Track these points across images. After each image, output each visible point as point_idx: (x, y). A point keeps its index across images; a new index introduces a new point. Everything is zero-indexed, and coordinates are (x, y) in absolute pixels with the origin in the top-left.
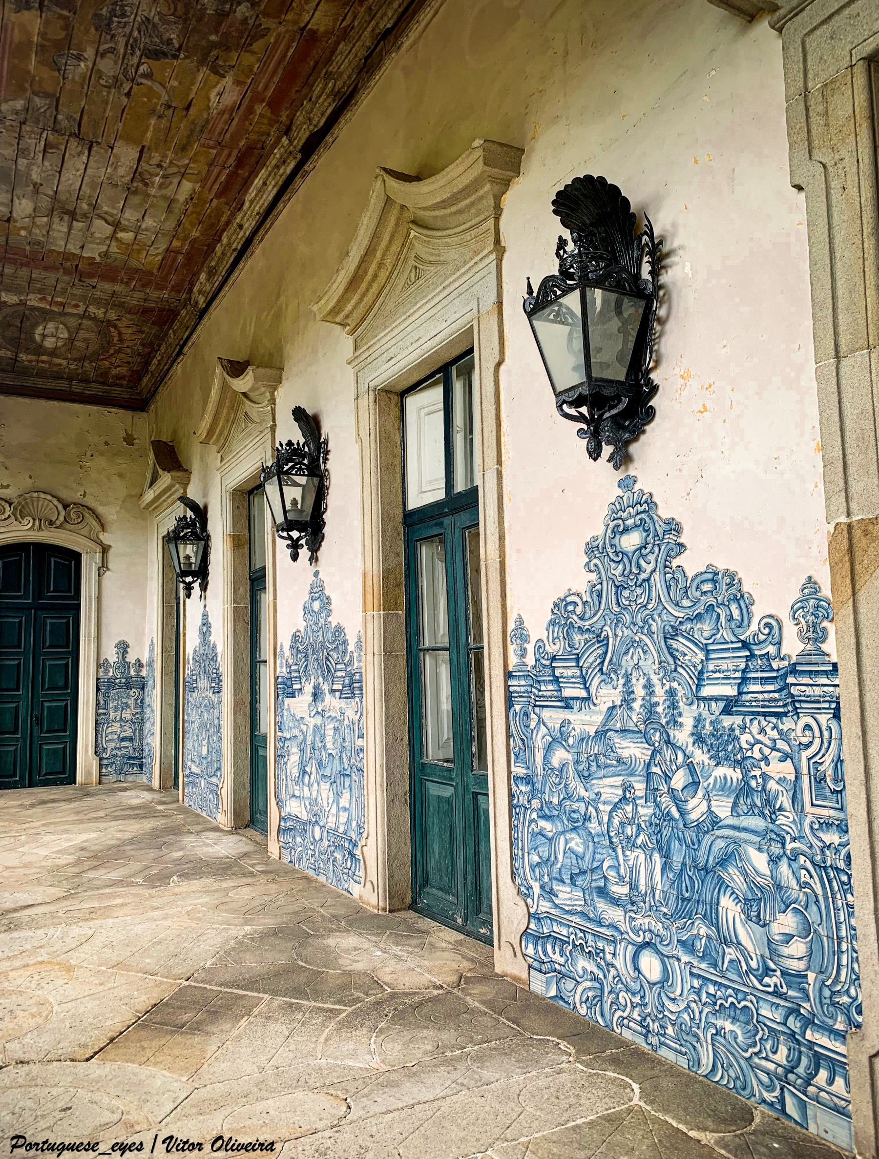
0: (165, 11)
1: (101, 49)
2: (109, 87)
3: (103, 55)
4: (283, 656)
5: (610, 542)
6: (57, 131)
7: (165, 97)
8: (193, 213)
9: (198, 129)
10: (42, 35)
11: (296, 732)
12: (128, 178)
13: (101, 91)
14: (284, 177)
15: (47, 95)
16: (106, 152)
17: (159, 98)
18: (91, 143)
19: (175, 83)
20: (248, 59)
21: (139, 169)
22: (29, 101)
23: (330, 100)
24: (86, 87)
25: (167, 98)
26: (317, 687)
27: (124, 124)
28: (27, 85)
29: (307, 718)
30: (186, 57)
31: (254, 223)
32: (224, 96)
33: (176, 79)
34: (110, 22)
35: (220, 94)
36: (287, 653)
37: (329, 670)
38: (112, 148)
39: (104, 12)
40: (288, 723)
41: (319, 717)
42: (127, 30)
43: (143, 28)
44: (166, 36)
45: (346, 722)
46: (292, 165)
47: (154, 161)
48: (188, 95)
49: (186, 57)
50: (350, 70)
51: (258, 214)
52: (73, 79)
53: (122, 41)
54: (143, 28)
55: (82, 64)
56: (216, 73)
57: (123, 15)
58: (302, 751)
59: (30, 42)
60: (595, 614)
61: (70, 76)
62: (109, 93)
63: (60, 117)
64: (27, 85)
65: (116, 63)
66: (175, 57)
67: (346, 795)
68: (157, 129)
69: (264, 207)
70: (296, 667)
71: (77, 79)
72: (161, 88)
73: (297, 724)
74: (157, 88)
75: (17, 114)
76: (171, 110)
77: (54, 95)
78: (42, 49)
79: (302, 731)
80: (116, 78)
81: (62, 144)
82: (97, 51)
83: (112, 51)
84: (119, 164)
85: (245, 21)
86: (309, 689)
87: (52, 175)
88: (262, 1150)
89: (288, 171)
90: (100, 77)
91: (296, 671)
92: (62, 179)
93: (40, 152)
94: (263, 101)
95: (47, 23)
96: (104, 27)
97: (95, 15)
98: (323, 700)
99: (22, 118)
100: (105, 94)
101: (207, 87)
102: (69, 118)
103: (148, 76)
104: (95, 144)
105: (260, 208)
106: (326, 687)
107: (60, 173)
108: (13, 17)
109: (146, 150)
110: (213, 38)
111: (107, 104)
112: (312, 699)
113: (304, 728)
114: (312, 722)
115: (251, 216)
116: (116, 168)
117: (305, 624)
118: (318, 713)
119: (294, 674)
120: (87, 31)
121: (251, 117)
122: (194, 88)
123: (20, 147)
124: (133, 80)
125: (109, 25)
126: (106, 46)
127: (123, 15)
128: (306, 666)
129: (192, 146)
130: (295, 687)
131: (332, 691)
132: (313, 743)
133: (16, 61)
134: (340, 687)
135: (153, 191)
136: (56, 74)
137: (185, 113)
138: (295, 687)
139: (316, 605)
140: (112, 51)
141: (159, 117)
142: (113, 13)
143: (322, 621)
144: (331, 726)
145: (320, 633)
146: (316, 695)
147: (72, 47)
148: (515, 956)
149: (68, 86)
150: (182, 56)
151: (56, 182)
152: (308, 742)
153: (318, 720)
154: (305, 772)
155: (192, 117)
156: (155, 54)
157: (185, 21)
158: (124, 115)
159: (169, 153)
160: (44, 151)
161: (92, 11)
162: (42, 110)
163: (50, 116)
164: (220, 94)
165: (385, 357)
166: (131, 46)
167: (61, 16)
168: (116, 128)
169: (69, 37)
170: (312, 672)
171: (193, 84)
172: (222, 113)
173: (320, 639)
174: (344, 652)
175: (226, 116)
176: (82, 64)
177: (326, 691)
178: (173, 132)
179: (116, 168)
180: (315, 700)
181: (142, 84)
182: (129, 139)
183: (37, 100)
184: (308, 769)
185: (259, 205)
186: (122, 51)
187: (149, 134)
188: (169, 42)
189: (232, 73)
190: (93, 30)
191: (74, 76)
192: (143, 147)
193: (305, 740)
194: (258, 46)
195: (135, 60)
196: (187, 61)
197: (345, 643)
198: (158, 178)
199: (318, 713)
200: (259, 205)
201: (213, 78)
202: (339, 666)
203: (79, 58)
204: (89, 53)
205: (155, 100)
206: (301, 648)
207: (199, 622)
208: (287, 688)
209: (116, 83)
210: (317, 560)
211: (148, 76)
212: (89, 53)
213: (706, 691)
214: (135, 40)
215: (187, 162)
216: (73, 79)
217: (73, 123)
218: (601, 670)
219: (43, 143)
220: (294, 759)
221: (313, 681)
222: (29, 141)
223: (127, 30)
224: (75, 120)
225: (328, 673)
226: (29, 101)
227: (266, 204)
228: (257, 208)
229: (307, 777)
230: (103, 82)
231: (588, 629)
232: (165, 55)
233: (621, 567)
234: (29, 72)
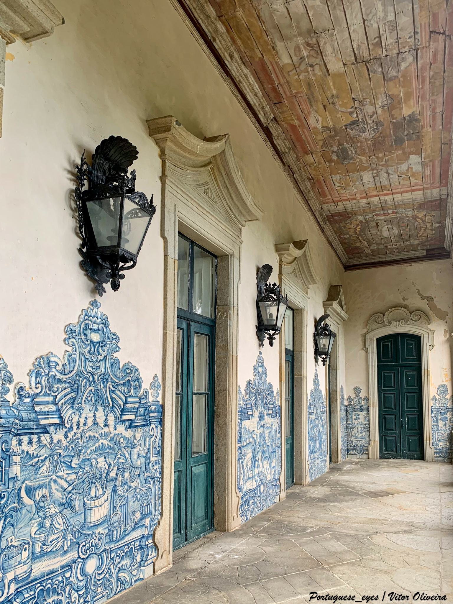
0: (360, 138)
1: (375, 114)
2: (364, 99)
3: (374, 113)
4: (241, 394)
5: (83, 332)
6: (378, 59)
7: (338, 107)
8: (262, 36)
9: (312, 99)
10: (401, 109)
11: (250, 440)
12: (322, 44)
13: (366, 95)
14: (258, 112)
15: (391, 79)
16: (346, 60)
17: (340, 105)
18: (357, 62)
19: (338, 116)
20: (320, 137)
21: (320, 56)
22: (398, 71)
23: (283, 150)
24: (374, 94)
25: (337, 107)
26: (261, 413)
27: (346, 83)
28: (401, 79)
29: (256, 430)
30: (342, 127)
31: (234, 74)
32: (315, 121)
33: (339, 118)
34: (377, 126)
35: (317, 120)
36: (243, 392)
37: (267, 404)
38: (344, 64)
39: (381, 128)
40: (245, 435)
41: (262, 428)
42: (369, 126)
43: (364, 129)
44: (354, 131)
45: (274, 428)
46: (262, 120)
47: (317, 68)
48: (329, 113)
49: (342, 127)
50: (289, 161)
51: (241, 82)
52: (381, 94)
53: (369, 121)
54: (364, 129)
55: (380, 104)
56: (326, 127)
57: (373, 130)
58: (254, 450)
59: (405, 103)
60: (69, 373)
61: (383, 95)
62: (363, 96)
63: (380, 70)
64: (401, 79)
65: (367, 112)
66: (346, 125)
67: (274, 460)
68: (329, 88)
69: (243, 88)
70: (250, 402)
71: (380, 96)
72: (343, 110)
73: (250, 435)
74: (344, 110)
75: (403, 58)
76: (330, 102)
77: (387, 81)
78: (400, 103)
79: (254, 438)
80: (364, 106)
81: (372, 50)
82: (377, 113)
83: (371, 117)
84: (334, 55)
85: (332, 146)
86: (257, 414)
87: (368, 15)
88: (323, 599)
89: (260, 116)
90: (370, 102)
91: (249, 403)
92: (360, 15)
93: (383, 34)
94: (299, 126)
95: (401, 114)
96: (378, 123)
97: (383, 125)
98: (264, 419)
99: (400, 57)
100: (364, 95)
101: (325, 119)
102: (375, 72)
103: (351, 113)
104: (354, 62)
105: (244, 86)
106: (265, 413)
107: (364, 21)
108: (414, 109)
109: (327, 74)
110: (338, 138)
111: (360, 89)
112: (258, 419)
113: (254, 436)
114: (258, 432)
115: (240, 75)
116: (334, 49)
117: (254, 377)
118: (261, 426)
119: (249, 406)
120: (384, 119)
121: (296, 118)
122: (329, 118)
123: (396, 32)
124: (356, 108)
125: (377, 125)
126: (374, 117)
127: (373, 130)
128: (256, 401)
129: (307, 89)
130: (249, 413)
131: (268, 414)
132: (259, 443)
133: (410, 90)
134: (271, 412)
135: (300, 40)
136: (390, 93)
137: (324, 104)
138: (249, 413)
139: (260, 370)
140: (371, 117)
141: (333, 95)
142: (377, 129)
143: (263, 379)
144: (268, 431)
145: (262, 385)
146: (261, 417)
147: (387, 110)
148: (169, 553)
149: (382, 89)
150: (344, 127)
151: (363, 9)
152: (257, 443)
153: (261, 430)
154: (255, 461)
155: (319, 103)
156: (354, 123)
157: (351, 138)
158: (349, 88)
159: (314, 78)
160: (380, 37)
161: (385, 126)
162: (390, 69)
163: (385, 67)
164: (317, 120)
165: (290, 290)
166: (364, 122)
167: (396, 118)
168: (349, 78)
169: (390, 112)
170: (259, 405)
171: (331, 119)
172: (309, 113)
173: (262, 388)
174: (273, 396)
175: (306, 112)
176: (380, 104)
177: (265, 415)
178: (321, 91)
179: (334, 49)
180: (260, 420)
181: (351, 108)
182: (340, 75)
183: (395, 74)
184: (257, 459)
185: (246, 86)
186: (367, 118)
187: (331, 84)
188: (352, 129)
189: (321, 130)
190: (382, 120)
191: (382, 97)
192: (329, 75)
193: (255, 443)
194: (321, 143)
195: (360, 117)
196: (340, 126)
197: (273, 392)
198: (305, 55)
199: (261, 426)
200: (246, 86)
201: (325, 125)
202: (271, 403)
203: (383, 106)
204: (379, 111)
205: (341, 103)
206: (252, 390)
207: (313, 377)
208: (244, 415)
209: (361, 103)
210: (263, 345)
211: (351, 113)
212: (379, 111)
213: (125, 418)
214: (364, 124)
215: (301, 77)
216: (381, 94)
217: (372, 69)
218: (72, 407)
219: (383, 44)
220: (249, 456)
221: (259, 409)
222: (392, 41)
223: (369, 126)
224: (372, 71)
225: (266, 405)
226: (398, 71)
227: (245, 91)
228: (245, 84)
229: (257, 463)
230: (368, 100)
231: (65, 381)
232: (350, 124)
233: (88, 348)
234: (402, 87)
